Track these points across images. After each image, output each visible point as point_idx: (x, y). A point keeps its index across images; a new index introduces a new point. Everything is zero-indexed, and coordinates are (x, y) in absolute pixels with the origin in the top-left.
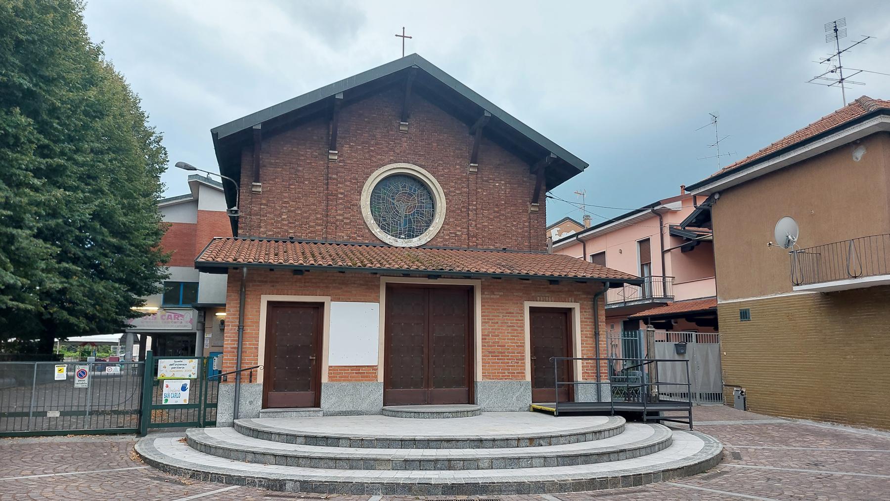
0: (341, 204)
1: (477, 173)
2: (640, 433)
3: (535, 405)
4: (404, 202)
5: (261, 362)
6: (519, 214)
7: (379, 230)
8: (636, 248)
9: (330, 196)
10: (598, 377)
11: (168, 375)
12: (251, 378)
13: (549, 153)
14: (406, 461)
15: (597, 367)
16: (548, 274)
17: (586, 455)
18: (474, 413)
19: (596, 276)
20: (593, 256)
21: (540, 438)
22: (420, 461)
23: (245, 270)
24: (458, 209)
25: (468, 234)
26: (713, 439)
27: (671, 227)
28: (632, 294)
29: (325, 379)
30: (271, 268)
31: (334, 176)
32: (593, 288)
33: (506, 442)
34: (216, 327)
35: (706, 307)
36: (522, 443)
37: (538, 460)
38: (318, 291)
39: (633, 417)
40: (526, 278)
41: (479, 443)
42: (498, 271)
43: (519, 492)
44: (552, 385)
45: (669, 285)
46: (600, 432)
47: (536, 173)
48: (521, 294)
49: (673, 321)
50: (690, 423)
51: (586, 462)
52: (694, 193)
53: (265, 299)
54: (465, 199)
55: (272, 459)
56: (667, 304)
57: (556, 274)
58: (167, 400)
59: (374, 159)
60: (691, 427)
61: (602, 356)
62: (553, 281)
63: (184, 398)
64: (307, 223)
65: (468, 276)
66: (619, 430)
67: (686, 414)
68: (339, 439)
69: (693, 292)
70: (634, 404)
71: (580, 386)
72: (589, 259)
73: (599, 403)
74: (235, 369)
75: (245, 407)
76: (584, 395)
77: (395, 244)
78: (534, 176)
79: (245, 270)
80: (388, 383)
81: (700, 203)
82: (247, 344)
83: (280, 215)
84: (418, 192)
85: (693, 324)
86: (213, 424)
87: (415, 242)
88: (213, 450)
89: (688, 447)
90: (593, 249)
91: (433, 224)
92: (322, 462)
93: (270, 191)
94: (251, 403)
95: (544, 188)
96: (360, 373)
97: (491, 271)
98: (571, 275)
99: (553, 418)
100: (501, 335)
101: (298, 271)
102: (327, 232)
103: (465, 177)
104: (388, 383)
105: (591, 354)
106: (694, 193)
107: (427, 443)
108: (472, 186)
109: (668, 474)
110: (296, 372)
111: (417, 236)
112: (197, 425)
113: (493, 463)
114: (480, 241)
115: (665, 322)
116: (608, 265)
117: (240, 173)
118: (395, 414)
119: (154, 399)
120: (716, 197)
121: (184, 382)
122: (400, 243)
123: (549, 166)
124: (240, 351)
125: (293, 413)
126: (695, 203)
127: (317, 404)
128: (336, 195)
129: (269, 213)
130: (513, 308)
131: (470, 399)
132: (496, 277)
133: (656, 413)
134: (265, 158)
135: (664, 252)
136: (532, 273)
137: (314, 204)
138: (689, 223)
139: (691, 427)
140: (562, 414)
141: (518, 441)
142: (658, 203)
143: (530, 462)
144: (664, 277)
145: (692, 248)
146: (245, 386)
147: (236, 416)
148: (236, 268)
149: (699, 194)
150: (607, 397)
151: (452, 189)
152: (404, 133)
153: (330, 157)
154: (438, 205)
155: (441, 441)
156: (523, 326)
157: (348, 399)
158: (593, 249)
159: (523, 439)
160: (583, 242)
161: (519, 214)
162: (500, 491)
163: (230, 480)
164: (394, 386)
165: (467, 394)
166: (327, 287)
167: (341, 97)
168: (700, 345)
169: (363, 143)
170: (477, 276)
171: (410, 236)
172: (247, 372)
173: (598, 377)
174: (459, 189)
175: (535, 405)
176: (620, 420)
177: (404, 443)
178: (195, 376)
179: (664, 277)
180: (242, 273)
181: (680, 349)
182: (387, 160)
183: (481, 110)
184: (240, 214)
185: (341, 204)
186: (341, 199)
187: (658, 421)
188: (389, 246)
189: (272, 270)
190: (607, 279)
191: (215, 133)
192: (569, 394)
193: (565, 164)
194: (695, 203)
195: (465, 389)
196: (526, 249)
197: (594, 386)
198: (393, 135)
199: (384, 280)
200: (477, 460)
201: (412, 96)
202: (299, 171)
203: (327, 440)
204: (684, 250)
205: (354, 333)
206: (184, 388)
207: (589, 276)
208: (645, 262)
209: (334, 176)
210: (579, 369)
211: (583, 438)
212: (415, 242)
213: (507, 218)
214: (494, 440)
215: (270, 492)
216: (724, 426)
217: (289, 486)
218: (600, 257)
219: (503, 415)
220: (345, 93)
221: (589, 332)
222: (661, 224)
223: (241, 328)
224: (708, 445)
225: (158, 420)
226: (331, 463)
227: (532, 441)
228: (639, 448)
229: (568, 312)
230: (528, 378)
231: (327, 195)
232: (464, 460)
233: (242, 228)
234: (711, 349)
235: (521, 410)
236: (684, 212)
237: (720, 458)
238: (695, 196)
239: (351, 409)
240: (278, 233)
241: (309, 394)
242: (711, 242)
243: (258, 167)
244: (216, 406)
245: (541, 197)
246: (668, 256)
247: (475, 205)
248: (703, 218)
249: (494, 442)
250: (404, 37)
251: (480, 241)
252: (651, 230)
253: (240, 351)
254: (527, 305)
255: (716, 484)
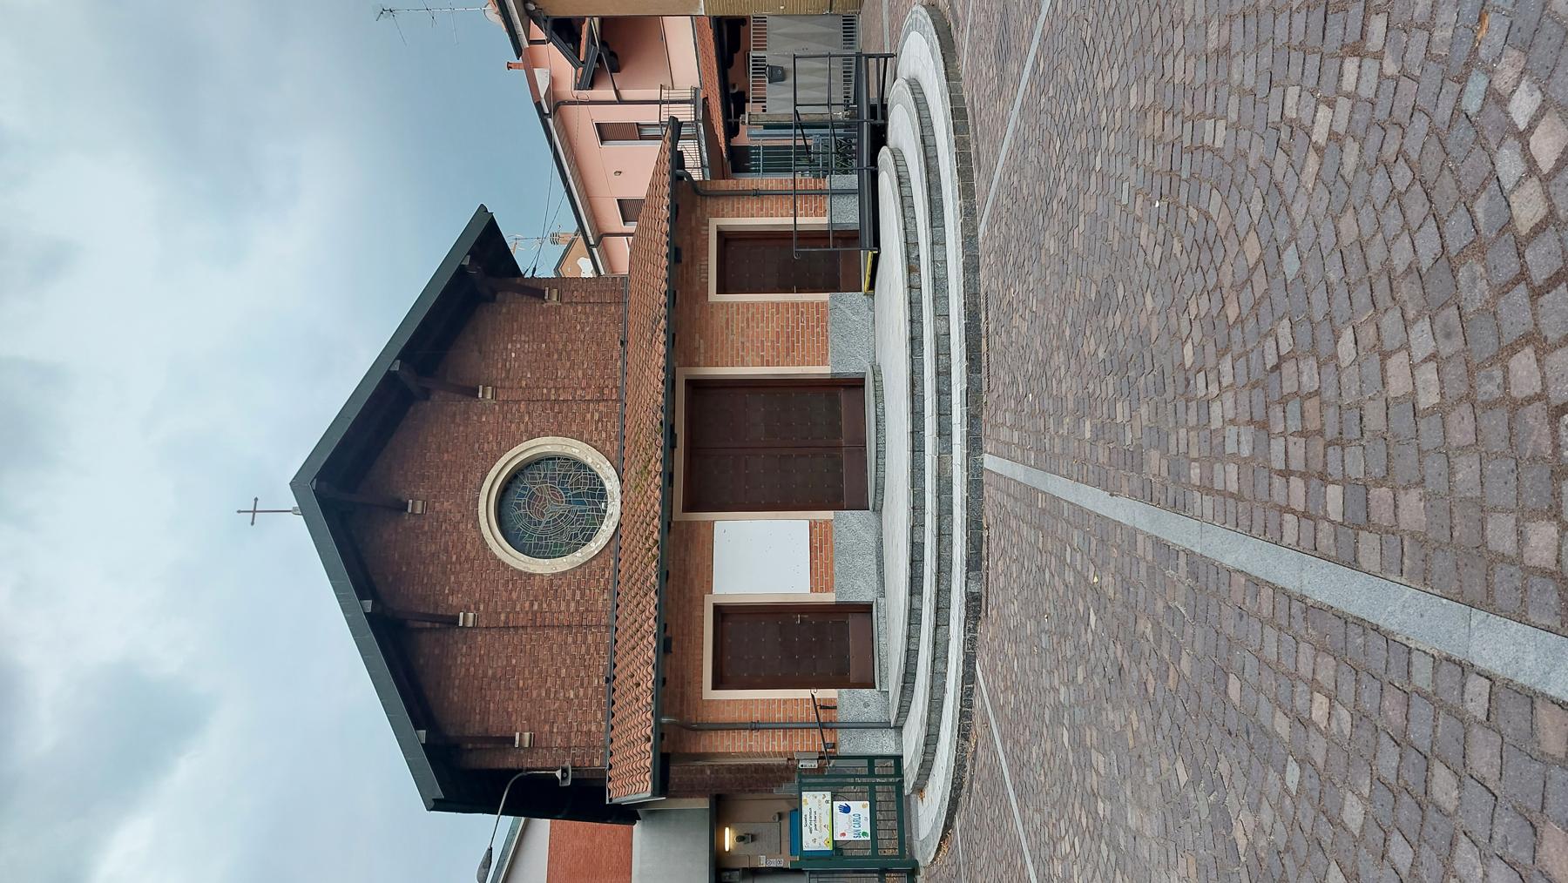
0: (549, 605)
1: (495, 388)
2: (901, 128)
3: (865, 286)
4: (545, 503)
5: (805, 694)
6: (562, 321)
7: (592, 544)
8: (613, 147)
9: (538, 624)
10: (822, 193)
11: (827, 834)
12: (829, 707)
13: (461, 267)
14: (939, 435)
15: (807, 193)
16: (665, 262)
17: (929, 189)
18: (877, 372)
19: (667, 189)
20: (625, 221)
21: (908, 257)
22: (939, 415)
23: (664, 720)
24: (555, 417)
25: (598, 401)
26: (908, 21)
27: (578, 87)
28: (691, 152)
29: (830, 598)
30: (661, 682)
31: (503, 617)
32: (685, 198)
33: (914, 305)
34: (750, 848)
35: (710, 34)
36: (915, 282)
37: (937, 253)
38: (697, 613)
39: (879, 137)
40: (672, 295)
41: (915, 341)
42: (662, 337)
43: (977, 269)
44: (835, 261)
45: (674, 95)
46: (899, 177)
47: (494, 293)
48: (697, 307)
49: (733, 91)
50: (886, 57)
51: (939, 188)
52: (526, 44)
53: (709, 694)
54: (538, 407)
55: (941, 630)
56: (706, 99)
57: (665, 249)
58: (864, 834)
59: (472, 555)
60: (892, 56)
61: (790, 186)
62: (676, 255)
63: (861, 808)
64: (582, 658)
65: (670, 384)
66: (897, 155)
67: (872, 62)
68: (913, 543)
69: (684, 57)
70: (860, 144)
71: (835, 220)
72: (631, 227)
73: (859, 192)
74: (817, 732)
75: (873, 714)
76: (848, 214)
77: (616, 517)
78: (499, 296)
79: (664, 720)
80: (836, 505)
81: (538, 33)
82: (779, 716)
83: (568, 700)
84: (527, 482)
85: (737, 57)
86: (898, 759)
87: (612, 485)
88: (933, 730)
89: (918, 55)
90: (612, 219)
91: (582, 457)
92: (944, 554)
93: (528, 720)
94: (866, 705)
95: (518, 280)
96: (820, 546)
97: (662, 349)
98: (666, 227)
99: (882, 255)
100: (760, 339)
101: (665, 646)
102: (598, 626)
103: (501, 407)
104: (835, 502)
105: (788, 203)
106: (526, 44)
107: (917, 414)
108: (517, 395)
109: (951, 74)
110: (818, 641)
111: (602, 484)
112: (900, 786)
113: (942, 315)
114: (610, 383)
115: (734, 102)
116: (643, 196)
117: (499, 770)
118: (880, 489)
119: (860, 853)
120: (532, 7)
121: (836, 809)
122: (614, 508)
123: (483, 271)
124: (787, 727)
125: (881, 641)
126: (543, 42)
127: (866, 609)
128: (535, 613)
129: (565, 719)
130: (721, 318)
131: (857, 384)
132: (672, 341)
133: (873, 109)
134: (475, 729)
135: (620, 101)
136: (664, 286)
137: (551, 649)
138: (573, 55)
139: (892, 56)
140: (876, 242)
141: (913, 287)
142: (538, 105)
143: (939, 264)
144: (660, 102)
145: (613, 54)
146: (842, 715)
147: (885, 726)
148: (662, 736)
149: (528, 37)
150: (851, 181)
151: (522, 427)
152: (426, 506)
153: (470, 624)
154: (548, 449)
155: (913, 395)
156: (747, 305)
157: (859, 562)
158: (612, 219)
159: (909, 280)
160: (601, 236)
161: (562, 321)
162: (976, 294)
163: (968, 677)
164: (841, 496)
165: (849, 390)
166: (690, 601)
167: (368, 604)
168: (770, 44)
169: (444, 573)
170: (670, 370)
171: (603, 495)
172: (822, 713)
173: (822, 193)
174: (522, 418)
175: (865, 286)
176: (884, 154)
177: (917, 448)
178: (828, 795)
179: (660, 102)
180: (670, 724)
181: (777, 75)
182: (474, 534)
183: (390, 377)
184: (568, 764)
185: (549, 605)
186: (540, 605)
187: (884, 107)
188: (620, 525)
189: (664, 681)
190: (672, 173)
191: (437, 805)
192: (848, 238)
193: (480, 242)
194: (543, 42)
195: (843, 395)
196: (622, 309)
197: (835, 199)
198: (431, 525)
199: (679, 515)
200: (937, 336)
201: (362, 489)
202: (494, 675)
203: (916, 562)
204: (616, 69)
205: (761, 557)
206: (846, 810)
207: (667, 200)
208: (636, 132)
209: (503, 617)
210: (811, 221)
211: (907, 200)
212: (612, 485)
213: (569, 340)
214: (912, 321)
215: (983, 614)
216: (890, 12)
217: (974, 588)
218: (628, 209)
219: (879, 335)
220: (361, 597)
221: (755, 204)
222: (574, 103)
223: (754, 727)
224: (915, 26)
225: (895, 843)
226: (945, 541)
227: (912, 268)
228: (920, 118)
229: (725, 238)
230: (825, 297)
231: (534, 627)
232: (937, 354)
233: (591, 761)
234: (776, 28)
235: (872, 309)
236: (556, 66)
237: (932, 8)
238: (531, 42)
239: (873, 557)
240: (599, 702)
241: (853, 621)
242: (603, 20)
243: (487, 739)
244: (871, 759)
245: (534, 285)
246: (627, 94)
247: (549, 390)
248: (565, 31)
249: (915, 321)
250: (254, 511)
251: (610, 383)
252: (584, 120)
253: (787, 727)
254: (714, 297)
255: (963, 8)
